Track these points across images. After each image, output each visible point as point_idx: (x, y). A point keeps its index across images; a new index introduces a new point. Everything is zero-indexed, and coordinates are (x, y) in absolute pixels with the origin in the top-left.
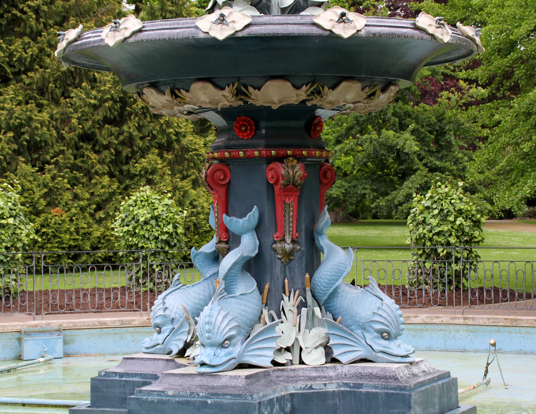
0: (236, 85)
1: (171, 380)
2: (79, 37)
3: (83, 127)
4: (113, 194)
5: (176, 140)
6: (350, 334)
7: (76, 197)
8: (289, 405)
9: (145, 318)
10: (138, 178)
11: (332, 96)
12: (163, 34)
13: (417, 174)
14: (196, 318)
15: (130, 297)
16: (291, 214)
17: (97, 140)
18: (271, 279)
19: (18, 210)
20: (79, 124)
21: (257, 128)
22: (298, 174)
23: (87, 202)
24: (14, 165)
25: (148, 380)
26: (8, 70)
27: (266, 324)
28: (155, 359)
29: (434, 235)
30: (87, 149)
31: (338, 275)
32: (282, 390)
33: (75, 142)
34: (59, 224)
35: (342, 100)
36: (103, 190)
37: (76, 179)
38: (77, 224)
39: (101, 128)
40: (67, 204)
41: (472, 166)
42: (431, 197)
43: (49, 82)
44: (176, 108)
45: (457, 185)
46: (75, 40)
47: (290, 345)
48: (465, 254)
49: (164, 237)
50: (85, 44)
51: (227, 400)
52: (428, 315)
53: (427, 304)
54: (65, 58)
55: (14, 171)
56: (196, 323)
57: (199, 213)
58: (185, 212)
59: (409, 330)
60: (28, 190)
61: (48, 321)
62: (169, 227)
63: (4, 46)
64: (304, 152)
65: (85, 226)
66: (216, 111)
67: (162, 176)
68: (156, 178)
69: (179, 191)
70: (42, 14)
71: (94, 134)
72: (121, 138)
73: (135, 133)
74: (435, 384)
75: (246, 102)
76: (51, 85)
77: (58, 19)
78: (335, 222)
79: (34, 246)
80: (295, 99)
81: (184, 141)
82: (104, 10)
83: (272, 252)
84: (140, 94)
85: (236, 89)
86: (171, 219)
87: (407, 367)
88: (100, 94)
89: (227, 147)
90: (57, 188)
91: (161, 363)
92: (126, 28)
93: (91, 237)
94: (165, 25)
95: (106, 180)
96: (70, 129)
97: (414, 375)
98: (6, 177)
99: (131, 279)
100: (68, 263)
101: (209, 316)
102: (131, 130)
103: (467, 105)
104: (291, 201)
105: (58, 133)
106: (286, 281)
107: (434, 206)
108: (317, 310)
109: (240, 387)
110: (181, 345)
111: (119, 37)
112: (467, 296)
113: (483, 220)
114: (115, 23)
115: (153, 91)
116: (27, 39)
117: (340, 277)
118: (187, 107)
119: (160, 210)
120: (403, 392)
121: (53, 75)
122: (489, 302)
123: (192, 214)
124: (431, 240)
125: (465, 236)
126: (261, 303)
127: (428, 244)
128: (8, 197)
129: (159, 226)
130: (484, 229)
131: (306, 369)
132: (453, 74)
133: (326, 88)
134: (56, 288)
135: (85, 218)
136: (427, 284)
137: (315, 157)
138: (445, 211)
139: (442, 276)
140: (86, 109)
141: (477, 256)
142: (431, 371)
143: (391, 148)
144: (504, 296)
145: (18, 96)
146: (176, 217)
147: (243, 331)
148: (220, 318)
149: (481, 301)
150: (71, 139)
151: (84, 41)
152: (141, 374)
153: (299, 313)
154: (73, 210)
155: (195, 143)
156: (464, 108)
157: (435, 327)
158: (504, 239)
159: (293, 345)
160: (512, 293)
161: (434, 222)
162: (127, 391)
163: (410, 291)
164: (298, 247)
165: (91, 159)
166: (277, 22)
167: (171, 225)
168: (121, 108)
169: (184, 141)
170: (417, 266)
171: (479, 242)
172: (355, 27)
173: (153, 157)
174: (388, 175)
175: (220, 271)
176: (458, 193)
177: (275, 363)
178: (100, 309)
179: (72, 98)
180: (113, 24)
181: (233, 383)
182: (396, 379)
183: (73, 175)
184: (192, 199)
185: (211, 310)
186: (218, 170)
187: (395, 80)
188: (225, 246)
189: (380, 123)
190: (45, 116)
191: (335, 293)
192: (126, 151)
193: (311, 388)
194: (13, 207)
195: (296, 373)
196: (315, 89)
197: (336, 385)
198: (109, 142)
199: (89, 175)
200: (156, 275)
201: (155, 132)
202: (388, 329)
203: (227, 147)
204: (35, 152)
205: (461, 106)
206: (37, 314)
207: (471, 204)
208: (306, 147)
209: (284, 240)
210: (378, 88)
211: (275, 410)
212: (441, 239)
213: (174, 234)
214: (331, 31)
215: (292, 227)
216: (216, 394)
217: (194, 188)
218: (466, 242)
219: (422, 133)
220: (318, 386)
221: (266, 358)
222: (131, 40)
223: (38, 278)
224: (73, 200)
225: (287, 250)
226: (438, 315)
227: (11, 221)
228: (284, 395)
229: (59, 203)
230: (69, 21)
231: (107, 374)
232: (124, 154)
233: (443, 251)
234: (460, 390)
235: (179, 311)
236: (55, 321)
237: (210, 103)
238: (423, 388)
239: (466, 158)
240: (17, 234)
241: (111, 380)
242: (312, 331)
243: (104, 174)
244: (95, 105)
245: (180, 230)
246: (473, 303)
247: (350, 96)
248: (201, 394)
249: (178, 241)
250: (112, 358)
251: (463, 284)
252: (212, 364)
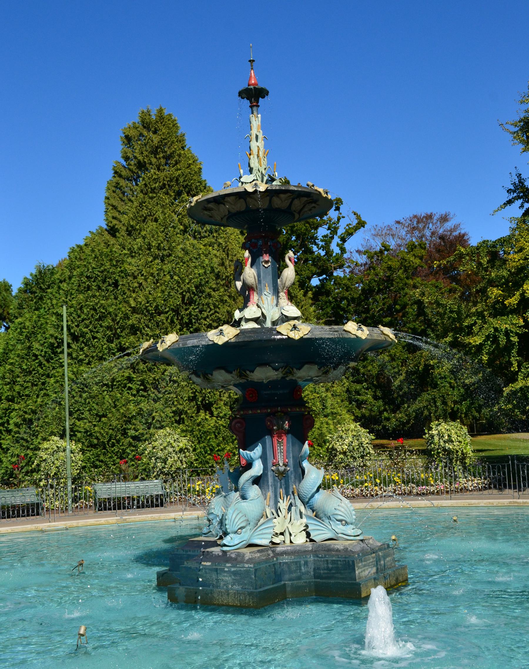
75: (247, 380)
85: (239, 372)
164: (288, 469)
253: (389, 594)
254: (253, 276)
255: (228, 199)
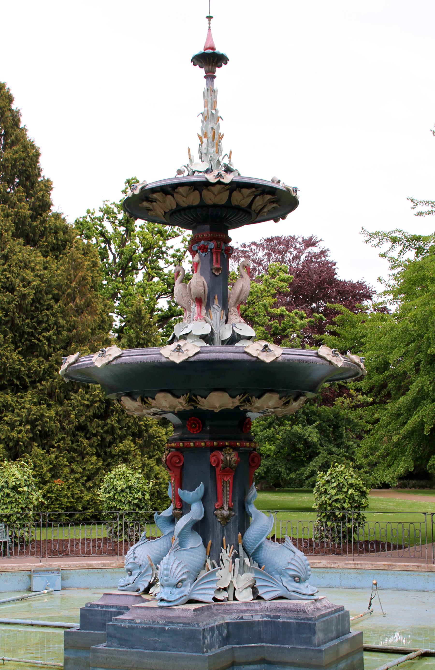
0: (188, 395)
1: (139, 611)
2: (76, 361)
3: (79, 421)
4: (99, 469)
5: (145, 430)
6: (271, 578)
7: (73, 471)
8: (226, 631)
9: (121, 562)
10: (117, 457)
11: (258, 403)
12: (136, 359)
13: (319, 456)
14: (173, 264)
15: (110, 546)
16: (228, 489)
17: (88, 430)
18: (213, 537)
19: (30, 481)
20: (76, 418)
21: (204, 425)
22: (233, 459)
23: (80, 475)
24: (30, 448)
25: (122, 611)
26: (27, 380)
27: (209, 570)
28: (127, 595)
29: (332, 502)
30: (81, 436)
31: (263, 533)
32: (220, 620)
33: (73, 432)
34: (60, 491)
35: (265, 406)
36: (92, 466)
37: (73, 458)
38: (72, 491)
39: (91, 421)
40: (66, 476)
41: (359, 452)
42: (331, 474)
43: (56, 389)
44: (145, 411)
45: (348, 464)
46: (74, 363)
47: (226, 586)
48: (355, 516)
49: (136, 502)
50: (81, 365)
51: (179, 627)
52: (328, 561)
53: (328, 553)
54: (66, 376)
55: (30, 453)
56: (157, 569)
57: (161, 483)
58: (151, 483)
59: (314, 572)
60: (39, 466)
61: (51, 563)
62: (139, 494)
63: (25, 363)
64: (238, 444)
65: (79, 492)
66: (173, 413)
67: (134, 456)
68: (130, 457)
69: (147, 467)
70: (52, 341)
71: (86, 425)
72: (106, 428)
73: (116, 425)
74: (333, 616)
75: (195, 407)
76: (57, 390)
77: (63, 345)
78: (260, 490)
79: (42, 507)
80: (231, 405)
81: (151, 431)
82: (95, 338)
83: (214, 517)
84: (119, 401)
85: (189, 397)
86: (140, 488)
87: (312, 603)
88: (92, 397)
89: (181, 439)
90: (59, 465)
91: (132, 598)
92: (110, 355)
93: (83, 501)
94: (138, 352)
95: (94, 459)
96: (69, 422)
97: (318, 609)
98: (24, 457)
99: (110, 532)
100: (66, 519)
101: (167, 564)
102: (113, 423)
103: (356, 407)
104: (228, 479)
105: (61, 424)
106: (224, 538)
107: (333, 481)
108: (247, 560)
109: (189, 618)
110: (146, 585)
111: (105, 361)
112: (356, 547)
113: (368, 491)
114: (102, 351)
115: (128, 398)
116: (41, 359)
117: (264, 535)
118: (153, 410)
119: (133, 481)
120: (310, 622)
121: (59, 383)
122: (372, 552)
123: (156, 484)
124: (330, 505)
125: (355, 503)
126: (205, 554)
127: (329, 508)
128: (24, 472)
129: (132, 494)
130: (368, 496)
131: (239, 604)
132: (345, 385)
133: (254, 398)
134: (56, 538)
135: (78, 486)
136: (327, 537)
137: (246, 447)
138: (341, 485)
139: (339, 532)
140: (82, 408)
141: (364, 517)
142: (330, 606)
143: (300, 438)
144: (383, 547)
145: (33, 398)
146: (144, 487)
147: (192, 575)
148: (175, 566)
149: (367, 551)
150: (70, 429)
151: (80, 363)
152: (117, 606)
153: (234, 562)
154: (70, 481)
155: (159, 432)
156: (353, 409)
157: (334, 570)
158: (383, 504)
159: (229, 586)
160: (389, 545)
161: (333, 492)
162: (107, 619)
163: (316, 543)
164: (233, 513)
165: (84, 444)
166: (219, 350)
167: (140, 493)
168: (106, 407)
169: (151, 431)
170: (320, 524)
171: (365, 507)
172: (275, 355)
173: (128, 442)
174: (299, 456)
175: (175, 530)
176: (350, 471)
177: (215, 599)
178: (88, 554)
179: (72, 400)
180: (101, 352)
181: (184, 615)
182: (304, 612)
183: (70, 455)
184: (156, 473)
185: (169, 559)
186: (175, 456)
187: (304, 393)
188: (179, 511)
189: (293, 419)
190: (52, 413)
191: (259, 548)
192: (109, 438)
193: (242, 618)
194: (28, 479)
195: (231, 607)
196: (246, 398)
197: (260, 616)
198: (97, 431)
199: (82, 455)
200: (129, 529)
201: (130, 424)
202: (299, 574)
203: (181, 439)
204: (45, 439)
205: (352, 408)
206: (43, 557)
207: (359, 479)
208: (239, 440)
209: (222, 508)
210: (291, 398)
211: (215, 635)
212: (338, 505)
213: (143, 500)
214: (257, 357)
215: (229, 498)
216: (172, 623)
217: (158, 465)
218: (356, 507)
219: (324, 427)
220: (247, 617)
221: (209, 596)
222: (113, 363)
223: (44, 530)
224: (70, 473)
225: (225, 515)
226: (336, 561)
227: (25, 489)
228: (222, 624)
229: (61, 475)
230: (71, 345)
231: (92, 605)
232: (108, 440)
233: (340, 514)
234: (351, 618)
235: (145, 559)
236: (55, 563)
237: (169, 407)
238: (325, 619)
239: (355, 446)
240: (30, 499)
241: (95, 610)
242: (243, 575)
243: (92, 454)
244: (88, 405)
245: (147, 496)
246: (361, 552)
247: (271, 403)
248: (160, 622)
249: (146, 504)
250: (97, 591)
251: (354, 538)
252: (168, 600)
253: (65, 649)
254: (202, 285)
255: (181, 189)
